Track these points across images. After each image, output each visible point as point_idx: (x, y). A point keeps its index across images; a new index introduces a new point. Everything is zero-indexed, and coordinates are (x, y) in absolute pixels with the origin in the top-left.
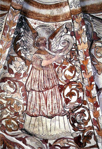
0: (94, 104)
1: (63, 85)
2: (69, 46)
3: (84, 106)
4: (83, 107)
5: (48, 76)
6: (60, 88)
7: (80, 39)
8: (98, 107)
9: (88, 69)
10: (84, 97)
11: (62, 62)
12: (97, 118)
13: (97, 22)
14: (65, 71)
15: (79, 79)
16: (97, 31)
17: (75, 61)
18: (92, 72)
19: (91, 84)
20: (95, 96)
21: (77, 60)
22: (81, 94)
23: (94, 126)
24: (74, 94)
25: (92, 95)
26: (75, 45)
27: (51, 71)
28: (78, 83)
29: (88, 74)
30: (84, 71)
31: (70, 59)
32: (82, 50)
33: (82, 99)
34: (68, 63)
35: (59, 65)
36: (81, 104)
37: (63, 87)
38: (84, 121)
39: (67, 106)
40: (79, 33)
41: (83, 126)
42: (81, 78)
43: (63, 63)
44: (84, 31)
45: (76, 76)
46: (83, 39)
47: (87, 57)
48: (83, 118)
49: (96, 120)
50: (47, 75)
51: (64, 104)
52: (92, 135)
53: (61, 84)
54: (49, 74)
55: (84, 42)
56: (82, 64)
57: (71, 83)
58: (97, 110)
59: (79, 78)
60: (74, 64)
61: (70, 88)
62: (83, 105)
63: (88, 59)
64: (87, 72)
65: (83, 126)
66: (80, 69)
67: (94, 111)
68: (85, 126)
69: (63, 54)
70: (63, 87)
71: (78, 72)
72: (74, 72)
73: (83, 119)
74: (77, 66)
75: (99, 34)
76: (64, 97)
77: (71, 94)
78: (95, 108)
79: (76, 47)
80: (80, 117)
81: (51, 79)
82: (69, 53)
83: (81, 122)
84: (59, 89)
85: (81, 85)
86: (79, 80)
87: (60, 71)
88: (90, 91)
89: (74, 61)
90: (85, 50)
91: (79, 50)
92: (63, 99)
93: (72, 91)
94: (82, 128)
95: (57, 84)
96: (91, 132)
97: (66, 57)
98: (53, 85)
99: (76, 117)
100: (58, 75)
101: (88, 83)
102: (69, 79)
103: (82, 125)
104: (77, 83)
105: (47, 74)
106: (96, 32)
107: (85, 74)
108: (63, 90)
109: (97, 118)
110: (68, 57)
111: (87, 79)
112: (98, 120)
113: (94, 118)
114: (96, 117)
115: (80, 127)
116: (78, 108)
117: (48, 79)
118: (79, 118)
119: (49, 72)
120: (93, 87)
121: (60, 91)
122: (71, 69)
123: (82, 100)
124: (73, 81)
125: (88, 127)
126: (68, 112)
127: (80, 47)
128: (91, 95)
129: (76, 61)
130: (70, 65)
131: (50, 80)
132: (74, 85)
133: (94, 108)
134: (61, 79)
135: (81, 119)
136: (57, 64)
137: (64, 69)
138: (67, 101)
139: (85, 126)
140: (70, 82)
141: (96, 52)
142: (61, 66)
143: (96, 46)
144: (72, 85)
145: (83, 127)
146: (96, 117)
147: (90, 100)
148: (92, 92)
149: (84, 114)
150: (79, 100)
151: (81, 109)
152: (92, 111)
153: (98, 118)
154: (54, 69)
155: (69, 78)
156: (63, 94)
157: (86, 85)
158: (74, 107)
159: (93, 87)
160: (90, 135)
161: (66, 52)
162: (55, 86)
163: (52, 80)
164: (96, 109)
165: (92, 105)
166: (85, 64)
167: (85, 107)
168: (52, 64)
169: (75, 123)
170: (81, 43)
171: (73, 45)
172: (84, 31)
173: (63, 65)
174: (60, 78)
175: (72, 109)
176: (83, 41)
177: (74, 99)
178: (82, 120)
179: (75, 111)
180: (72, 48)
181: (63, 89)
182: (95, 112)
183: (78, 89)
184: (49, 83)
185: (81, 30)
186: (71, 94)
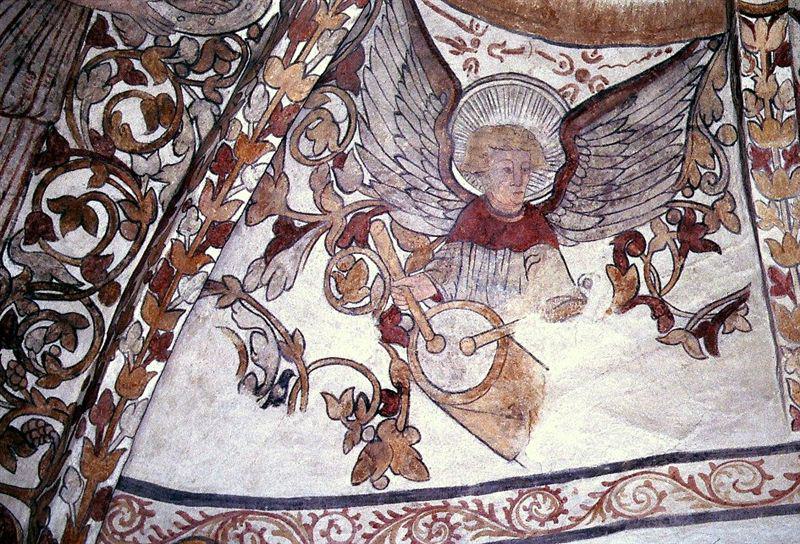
0: (154, 339)
1: (73, 144)
2: (230, 14)
3: (98, 303)
4: (90, 306)
5: (29, 45)
6: (44, 147)
7: (302, 45)
8: (159, 361)
9: (238, 182)
10: (123, 265)
11: (143, 47)
12: (123, 399)
13: (399, 19)
14: (126, 95)
15: (160, 180)
16: (374, 53)
17: (202, 96)
18: (243, 206)
19: (202, 249)
20: (178, 310)
21: (214, 96)
22: (120, 247)
23: (89, 423)
24: (89, 223)
25: (176, 295)
26: (255, 31)
27: (60, 40)
28: (143, 191)
29: (222, 205)
30: (215, 178)
31: (189, 67)
32: (272, 92)
33: (109, 270)
34: (165, 72)
35: (121, 46)
36: (88, 286)
37: (62, 154)
38: (52, 366)
39: (24, 248)
40: (318, 19)
41: (31, 379)
42: (169, 183)
43: (143, 52)
44: (341, 27)
45: (154, 159)
46: (314, 52)
47: (271, 138)
48: (54, 351)
49: (116, 403)
50: (25, 37)
51: (15, 231)
52: (45, 442)
53: (62, 127)
54: (38, 42)
55: (309, 68)
56: (231, 144)
57: (110, 166)
58: (149, 368)
59: (160, 176)
60: (187, 100)
61: (93, 182)
62: (94, 297)
63: (268, 146)
64: (225, 190)
65: (31, 379)
66: (200, 145)
67: (132, 365)
68: (41, 390)
69: (174, 20)
70: (62, 154)
71: (181, 149)
72: (160, 131)
73: (50, 354)
74: (194, 120)
75: (370, 69)
76: (36, 200)
77: (75, 212)
78: (148, 353)
79: (251, 43)
80: (45, 338)
81: (29, 71)
82: (201, 41)
83: (36, 360)
84: (38, 147)
85: (149, 210)
86: (157, 186)
87: (102, 73)
88: (180, 275)
89: (198, 90)
90: (286, 102)
91: (265, 84)
92: (26, 209)
93: (91, 204)
94: (22, 389)
95: (42, 119)
96: (47, 425)
97: (178, 43)
98: (21, 103)
99: (28, 323)
100: (76, 83)
101: (192, 238)
102: (117, 144)
103: (29, 376)
104: (140, 187)
105: (30, 32)
106: (367, 51)
107: (211, 193)
108: (55, 168)
109: (123, 399)
110: (188, 51)
111: (203, 218)
112: (120, 409)
113: (113, 390)
114: (124, 392)
115: (15, 380)
116: (67, 293)
117: (20, 61)
118: (38, 336)
119: (45, 33)
120: (199, 266)
121: (37, 161)
122: (158, 112)
123: (108, 275)
124: (129, 165)
125: (48, 401)
126: (11, 279)
127: (274, 71)
128: (171, 294)
129: (207, 99)
130: (167, 88)
131: (23, 71)
132: (118, 186)
133: (141, 354)
134: (77, 112)
135: (46, 348)
136: (112, 32)
137: (126, 82)
138: (39, 229)
139: (41, 390)
140: (112, 159)
141: (306, 127)
142: (121, 58)
143: (325, 106)
144: (112, 176)
145: (29, 389)
146: (124, 392)
147: (151, 306)
148: (180, 285)
149: (71, 335)
150: (95, 263)
151: (77, 307)
152: (127, 359)
153: (129, 402)
154: (80, 44)
155: (117, 140)
156: (43, 185)
157: (182, 238)
158: (53, 277)
159: (199, 266)
160: (34, 440)
161: (192, 23)
162: (28, 122)
163: (35, 82)
164: (148, 361)
165: (145, 335)
166: (242, 153)
167: (97, 309)
168: (86, 13)
169: (9, 348)
170: (296, 62)
171: (249, 27)
172: (341, 27)
173: (137, 65)
174: (76, 103)
175: (34, 280)
176: (307, 61)
177: (77, 243)
178: (43, 357)
179: (43, 297)
180: (233, 34)
181: (58, 163)
182: (134, 368)
183: (123, 217)
184: (9, 84)
185: (337, 14)
186: (75, 212)
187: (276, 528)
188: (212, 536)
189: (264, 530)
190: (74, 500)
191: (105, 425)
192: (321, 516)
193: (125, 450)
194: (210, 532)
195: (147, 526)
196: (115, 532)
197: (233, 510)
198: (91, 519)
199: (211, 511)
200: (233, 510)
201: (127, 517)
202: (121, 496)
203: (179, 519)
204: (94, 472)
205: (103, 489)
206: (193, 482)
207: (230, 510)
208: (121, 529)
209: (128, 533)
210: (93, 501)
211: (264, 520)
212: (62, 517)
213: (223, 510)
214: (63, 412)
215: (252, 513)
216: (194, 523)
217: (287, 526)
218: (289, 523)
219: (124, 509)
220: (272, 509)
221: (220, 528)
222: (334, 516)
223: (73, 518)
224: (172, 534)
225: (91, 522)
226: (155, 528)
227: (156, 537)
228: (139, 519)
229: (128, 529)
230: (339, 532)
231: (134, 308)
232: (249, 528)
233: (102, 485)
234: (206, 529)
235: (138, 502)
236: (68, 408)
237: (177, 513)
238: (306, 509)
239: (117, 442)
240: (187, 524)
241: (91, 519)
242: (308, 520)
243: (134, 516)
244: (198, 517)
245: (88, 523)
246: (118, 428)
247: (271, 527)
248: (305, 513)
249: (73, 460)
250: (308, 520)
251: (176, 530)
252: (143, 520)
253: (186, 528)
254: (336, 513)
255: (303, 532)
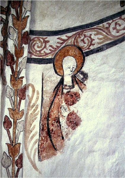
187: (96, 33)
188: (72, 43)
189: (91, 35)
190: (15, 38)
191: (18, 8)
192: (112, 23)
193: (28, 16)
194: (71, 42)
195: (48, 46)
196: (36, 51)
197: (78, 31)
198: (23, 44)
199: (69, 34)
200: (78, 31)
201: (40, 45)
202: (35, 38)
203: (59, 41)
204: (19, 26)
205: (25, 33)
206: (60, 26)
207: (76, 32)
208: (38, 49)
209: (41, 50)
210: (23, 38)
211: (90, 31)
212: (12, 45)
213: (74, 33)
214: (5, 11)
215: (86, 30)
216: (64, 41)
217: (99, 30)
218: (100, 29)
219: (38, 42)
220: (92, 27)
221: (75, 39)
222: (117, 21)
223: (16, 45)
224: (58, 47)
225: (24, 45)
226: (51, 46)
227: (52, 49)
228: (44, 44)
229: (41, 49)
230: (120, 26)
231: (35, 35)
232: (85, 36)
233: (24, 31)
234: (69, 41)
235: (42, 38)
236: (5, 9)
237: (57, 39)
238: (105, 22)
239: (24, 14)
240: (62, 42)
241: (23, 44)
242: (107, 26)
243: (42, 43)
244: (66, 38)
245: (23, 46)
246: (23, 8)
247: (93, 33)
248: (105, 24)
249: (10, 24)
250: (107, 26)
251: (59, 45)
252: (46, 44)
253: (62, 43)
254: (117, 19)
255: (106, 31)
